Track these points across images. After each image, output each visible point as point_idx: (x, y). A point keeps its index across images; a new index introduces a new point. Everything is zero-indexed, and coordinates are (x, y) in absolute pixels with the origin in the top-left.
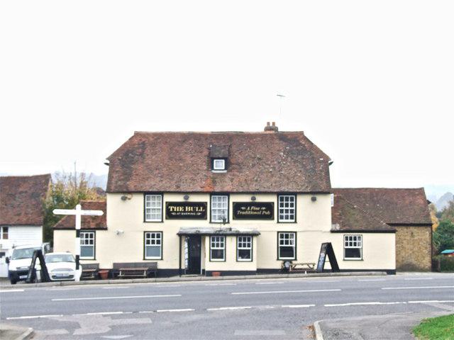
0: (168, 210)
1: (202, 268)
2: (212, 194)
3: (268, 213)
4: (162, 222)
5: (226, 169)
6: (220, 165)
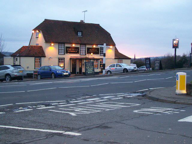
0: (66, 50)
1: (82, 72)
2: (81, 44)
3: (97, 52)
4: (64, 54)
5: (82, 35)
6: (80, 34)
